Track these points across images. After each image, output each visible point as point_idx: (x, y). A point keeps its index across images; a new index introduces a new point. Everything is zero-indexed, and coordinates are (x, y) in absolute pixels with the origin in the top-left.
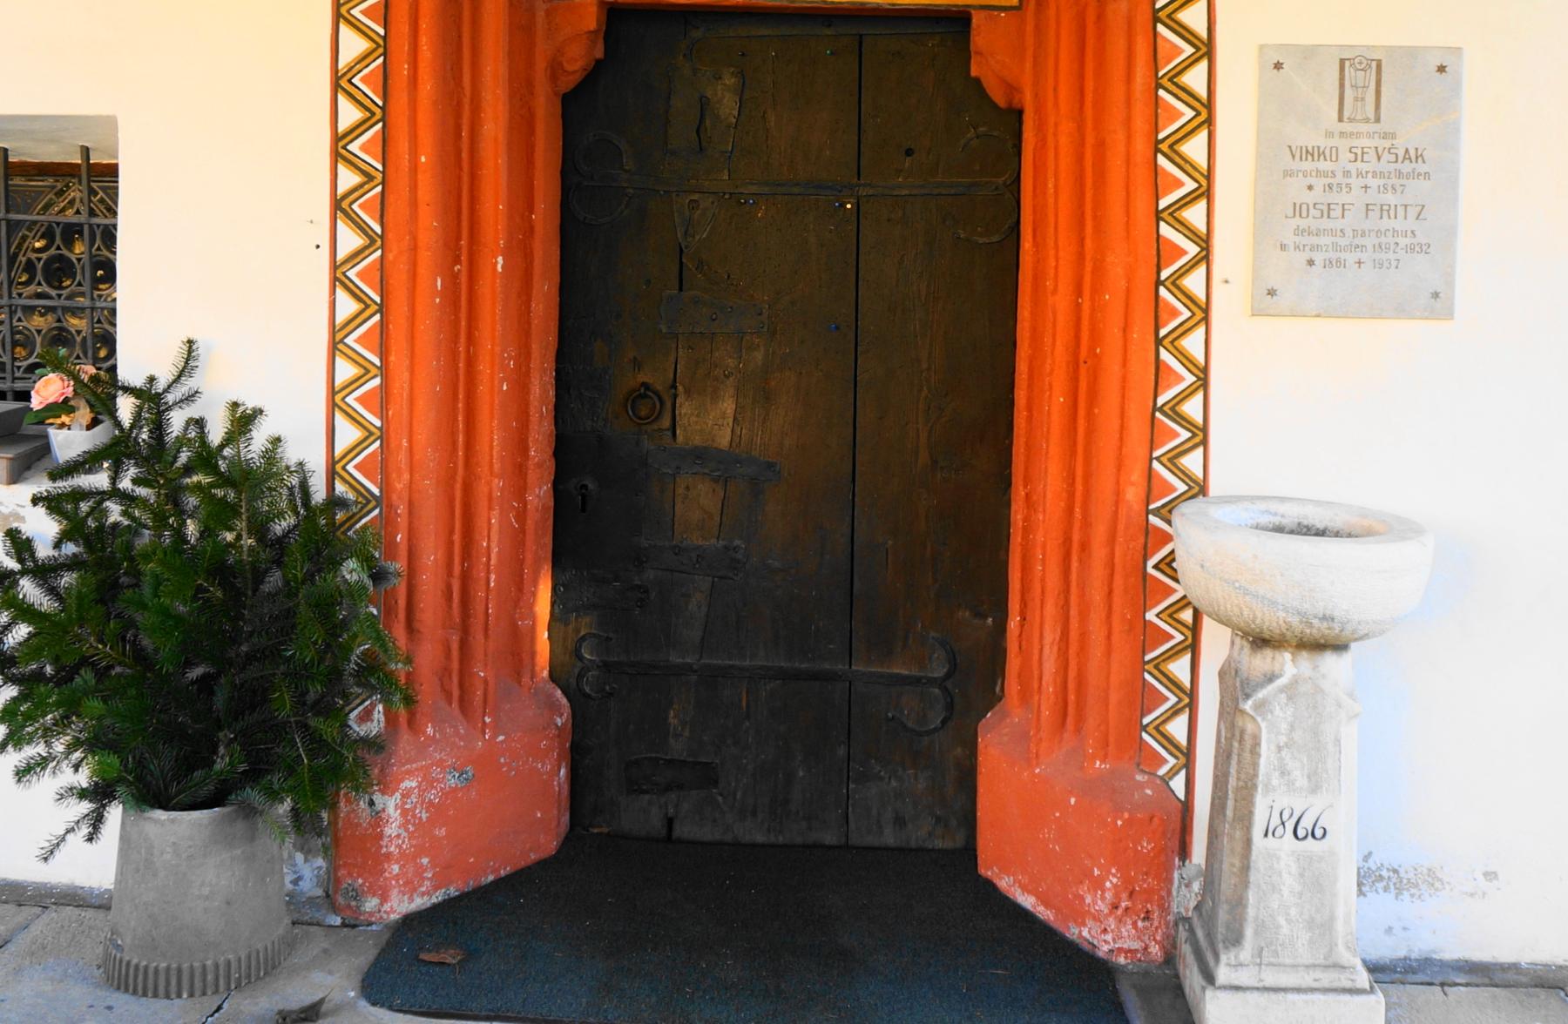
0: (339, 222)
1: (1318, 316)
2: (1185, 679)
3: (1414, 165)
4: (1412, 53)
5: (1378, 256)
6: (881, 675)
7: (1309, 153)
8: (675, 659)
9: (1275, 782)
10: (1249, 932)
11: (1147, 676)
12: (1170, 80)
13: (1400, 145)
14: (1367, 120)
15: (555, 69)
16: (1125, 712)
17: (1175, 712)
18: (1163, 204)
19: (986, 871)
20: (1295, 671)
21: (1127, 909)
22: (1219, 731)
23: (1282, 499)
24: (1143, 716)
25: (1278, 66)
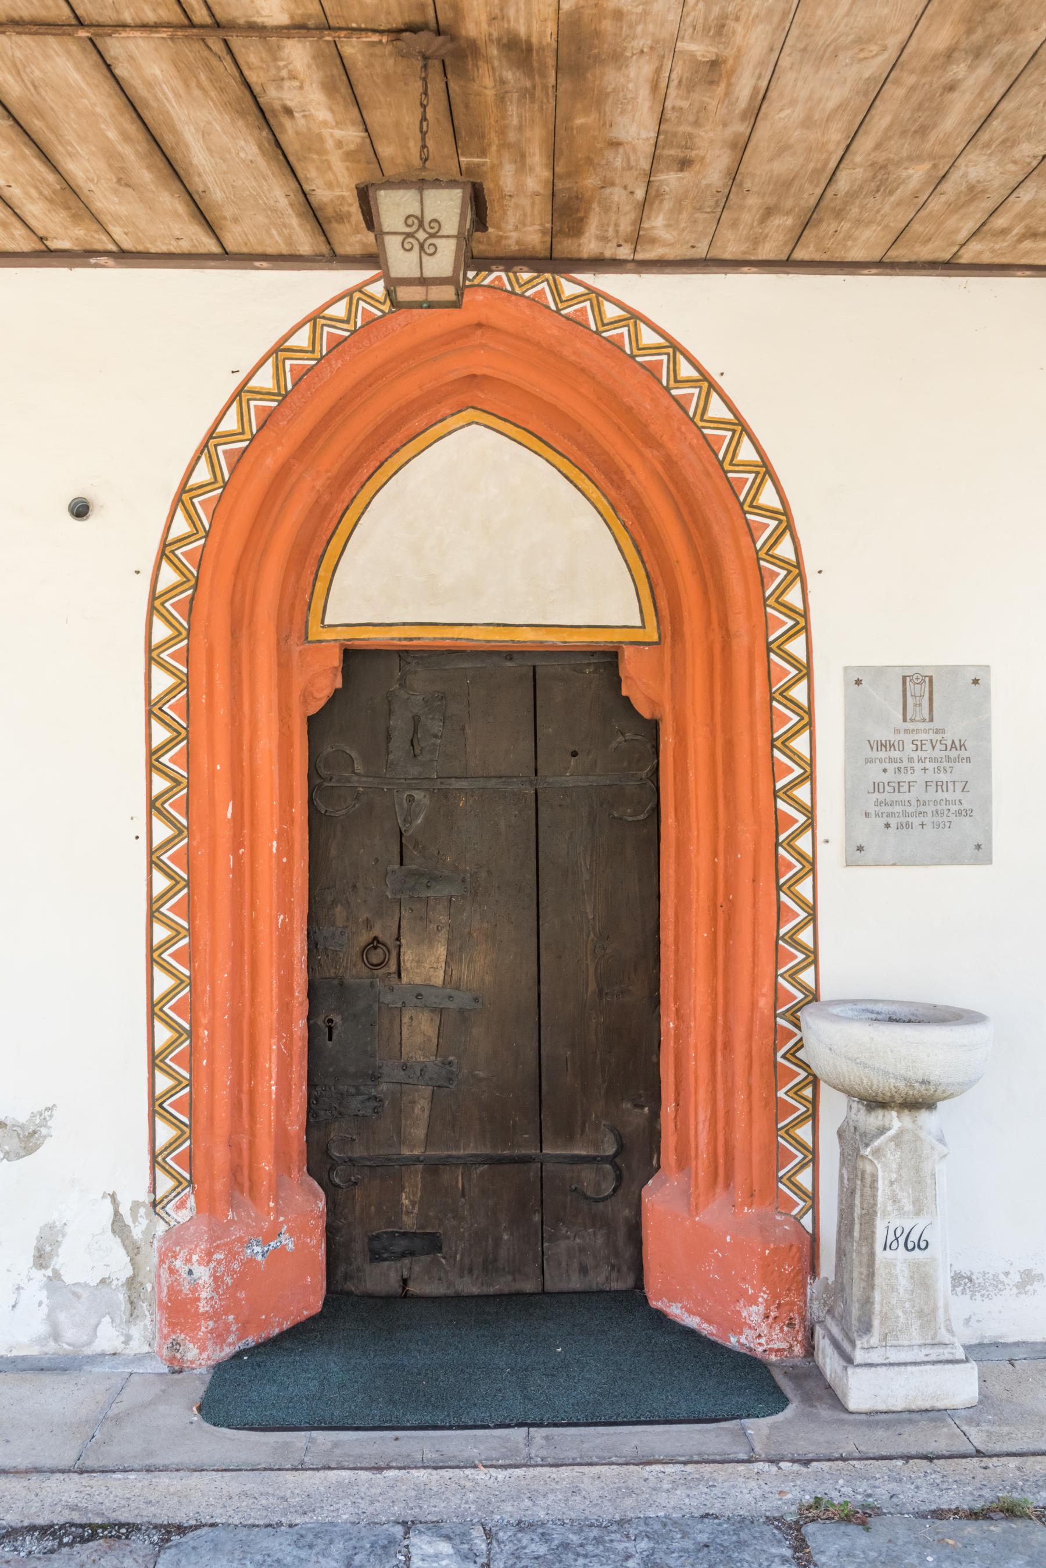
0: (154, 818)
1: (894, 864)
2: (808, 1140)
3: (959, 752)
4: (954, 671)
5: (936, 819)
6: (565, 1157)
7: (883, 745)
8: (406, 1152)
9: (889, 1208)
10: (876, 1323)
11: (780, 1140)
12: (781, 694)
13: (949, 737)
14: (924, 720)
15: (306, 697)
16: (763, 1168)
17: (802, 1166)
18: (779, 785)
19: (656, 1304)
20: (900, 1124)
21: (776, 1318)
22: (841, 1176)
23: (876, 1001)
24: (778, 1170)
25: (858, 682)
